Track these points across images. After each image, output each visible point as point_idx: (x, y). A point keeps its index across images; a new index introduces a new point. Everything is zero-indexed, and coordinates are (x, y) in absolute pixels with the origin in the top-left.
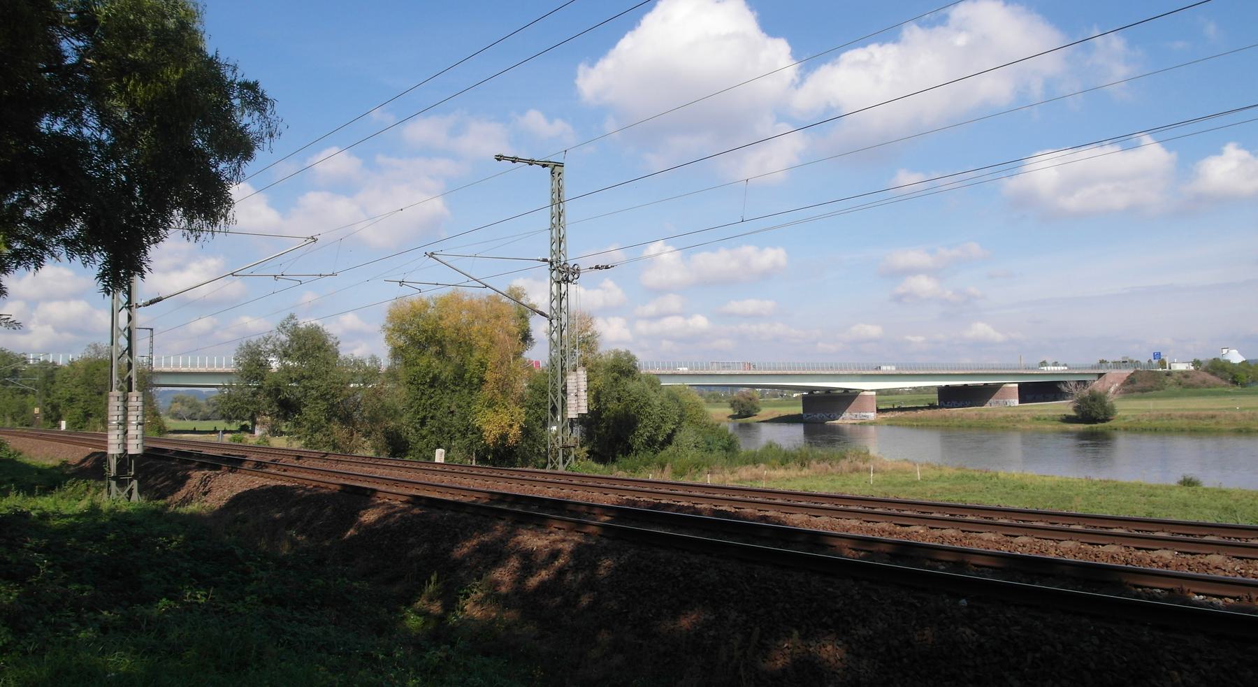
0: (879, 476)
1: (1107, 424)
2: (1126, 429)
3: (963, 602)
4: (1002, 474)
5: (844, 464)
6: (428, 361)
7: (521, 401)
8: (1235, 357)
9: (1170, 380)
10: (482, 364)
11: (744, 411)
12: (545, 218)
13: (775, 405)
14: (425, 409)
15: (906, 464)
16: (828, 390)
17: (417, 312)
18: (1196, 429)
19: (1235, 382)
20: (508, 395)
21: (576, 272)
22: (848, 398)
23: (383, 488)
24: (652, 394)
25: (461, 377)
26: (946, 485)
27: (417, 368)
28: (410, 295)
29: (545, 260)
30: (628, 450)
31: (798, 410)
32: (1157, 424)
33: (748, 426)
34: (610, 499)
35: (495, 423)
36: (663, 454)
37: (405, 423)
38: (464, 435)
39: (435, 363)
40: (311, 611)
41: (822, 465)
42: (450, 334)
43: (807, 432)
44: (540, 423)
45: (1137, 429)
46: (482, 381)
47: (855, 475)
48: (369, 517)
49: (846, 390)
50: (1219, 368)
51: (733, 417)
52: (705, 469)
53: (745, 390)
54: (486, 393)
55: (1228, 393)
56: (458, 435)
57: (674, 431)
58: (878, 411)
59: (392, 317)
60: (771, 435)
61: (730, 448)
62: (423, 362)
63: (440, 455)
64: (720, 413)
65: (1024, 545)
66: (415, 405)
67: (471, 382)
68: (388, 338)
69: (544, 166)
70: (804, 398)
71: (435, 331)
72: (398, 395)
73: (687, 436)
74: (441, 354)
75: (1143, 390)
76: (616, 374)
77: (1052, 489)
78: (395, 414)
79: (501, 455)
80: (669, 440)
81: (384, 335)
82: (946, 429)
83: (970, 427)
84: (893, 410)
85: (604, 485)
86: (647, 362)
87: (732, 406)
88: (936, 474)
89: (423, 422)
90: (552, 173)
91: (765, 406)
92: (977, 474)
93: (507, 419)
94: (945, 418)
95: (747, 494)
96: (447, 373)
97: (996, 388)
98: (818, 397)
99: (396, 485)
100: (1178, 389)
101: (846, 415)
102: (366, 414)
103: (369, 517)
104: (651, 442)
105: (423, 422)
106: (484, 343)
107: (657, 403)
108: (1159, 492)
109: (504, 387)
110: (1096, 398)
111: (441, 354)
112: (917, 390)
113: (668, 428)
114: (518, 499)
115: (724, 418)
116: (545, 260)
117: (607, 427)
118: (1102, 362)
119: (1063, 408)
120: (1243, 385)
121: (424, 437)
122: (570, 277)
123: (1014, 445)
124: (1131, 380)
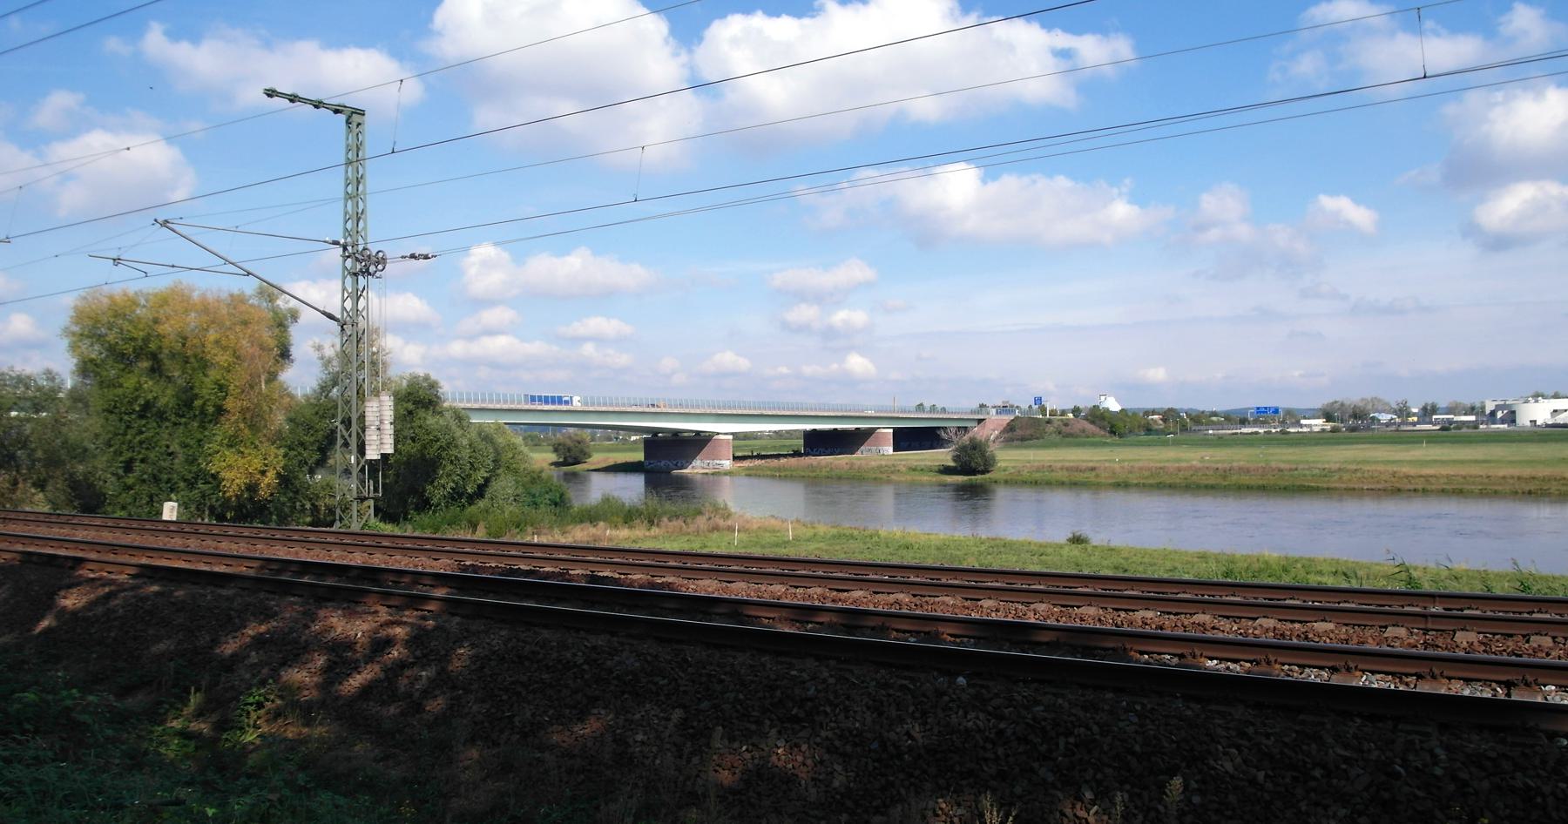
0: (744, 536)
1: (987, 476)
2: (1006, 482)
3: (961, 680)
4: (883, 533)
5: (701, 521)
6: (138, 381)
7: (277, 438)
8: (1113, 405)
9: (1050, 428)
10: (221, 388)
11: (571, 455)
12: (335, 183)
13: (610, 450)
14: (131, 448)
15: (773, 521)
16: (676, 433)
17: (120, 311)
18: (1077, 482)
19: (1113, 432)
20: (259, 430)
21: (381, 261)
22: (698, 443)
23: (93, 556)
24: (459, 433)
25: (188, 404)
26: (822, 545)
27: (120, 391)
28: (126, 283)
29: (336, 243)
30: (424, 505)
31: (639, 456)
32: (1037, 476)
33: (575, 474)
34: (443, 565)
35: (239, 469)
36: (472, 509)
37: (102, 470)
38: (191, 485)
39: (148, 384)
40: (19, 743)
41: (675, 523)
42: (171, 342)
43: (648, 483)
44: (305, 469)
45: (1016, 482)
46: (220, 411)
47: (715, 535)
48: (71, 601)
49: (698, 433)
50: (1098, 416)
51: (556, 464)
52: (530, 529)
53: (571, 430)
54: (227, 427)
55: (1105, 444)
56: (182, 484)
57: (487, 480)
58: (735, 458)
59: (80, 316)
60: (600, 488)
61: (560, 504)
62: (130, 382)
63: (170, 511)
64: (542, 459)
65: (990, 609)
66: (116, 441)
67: (203, 412)
68: (73, 347)
69: (336, 111)
70: (646, 441)
71: (146, 340)
72: (86, 427)
73: (504, 486)
74: (156, 370)
75: (1023, 439)
76: (411, 406)
77: (938, 549)
78: (83, 454)
79: (249, 510)
80: (481, 492)
81: (66, 342)
82: (813, 481)
83: (840, 478)
84: (752, 457)
85: (422, 550)
86: (454, 391)
87: (556, 450)
88: (810, 532)
89: (128, 466)
90: (348, 122)
91: (599, 451)
92: (856, 533)
93: (257, 463)
94: (811, 468)
95: (627, 555)
96: (166, 398)
97: (869, 433)
98: (664, 441)
99: (108, 554)
100: (1058, 438)
101: (697, 463)
102: (39, 454)
103: (71, 601)
104: (456, 495)
105: (128, 466)
106: (223, 358)
107: (465, 442)
108: (1050, 550)
109: (254, 419)
110: (976, 447)
111: (156, 370)
112: (778, 434)
113: (481, 474)
114: (306, 567)
115: (545, 465)
116: (336, 243)
117: (397, 475)
118: (982, 406)
119: (941, 457)
120: (1121, 436)
121: (130, 488)
122: (372, 269)
123: (886, 499)
124: (1010, 427)
